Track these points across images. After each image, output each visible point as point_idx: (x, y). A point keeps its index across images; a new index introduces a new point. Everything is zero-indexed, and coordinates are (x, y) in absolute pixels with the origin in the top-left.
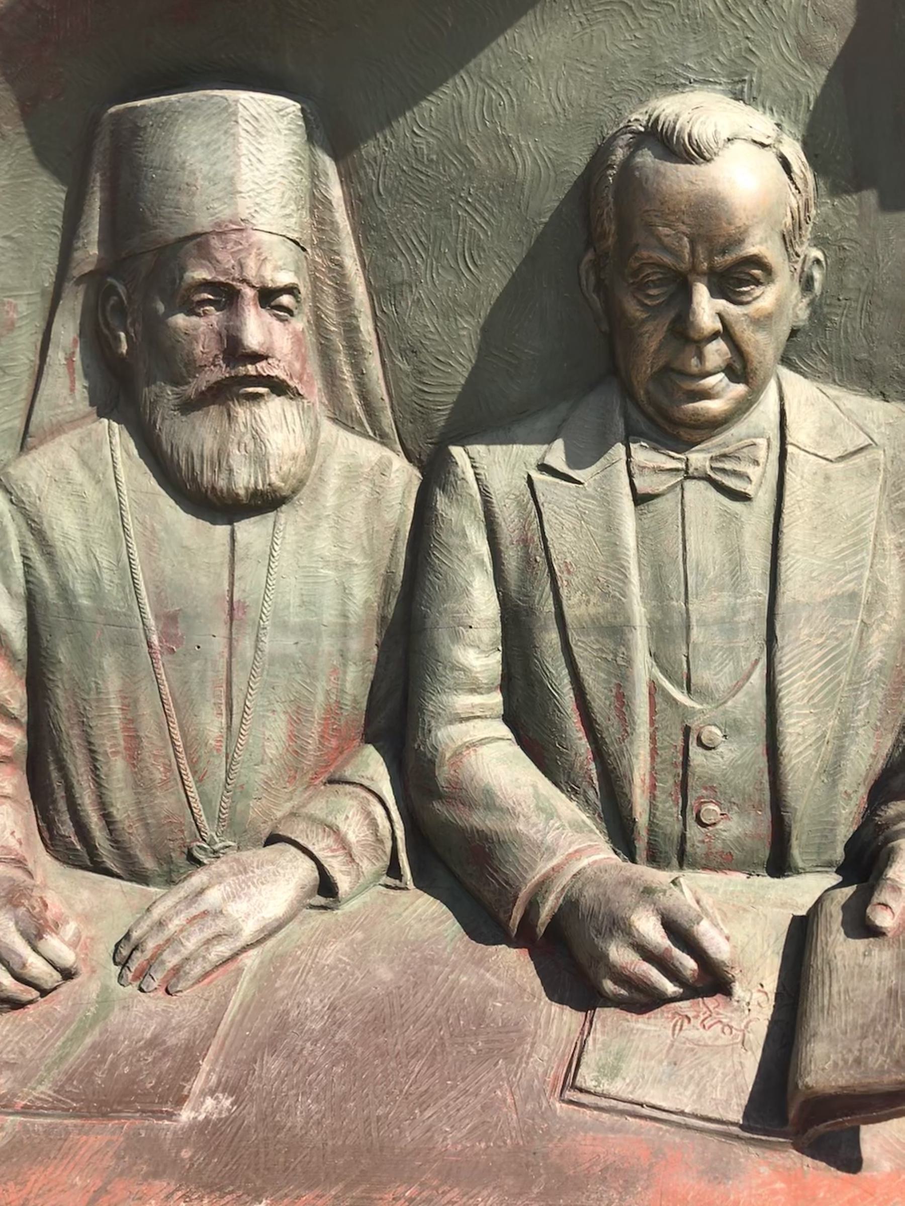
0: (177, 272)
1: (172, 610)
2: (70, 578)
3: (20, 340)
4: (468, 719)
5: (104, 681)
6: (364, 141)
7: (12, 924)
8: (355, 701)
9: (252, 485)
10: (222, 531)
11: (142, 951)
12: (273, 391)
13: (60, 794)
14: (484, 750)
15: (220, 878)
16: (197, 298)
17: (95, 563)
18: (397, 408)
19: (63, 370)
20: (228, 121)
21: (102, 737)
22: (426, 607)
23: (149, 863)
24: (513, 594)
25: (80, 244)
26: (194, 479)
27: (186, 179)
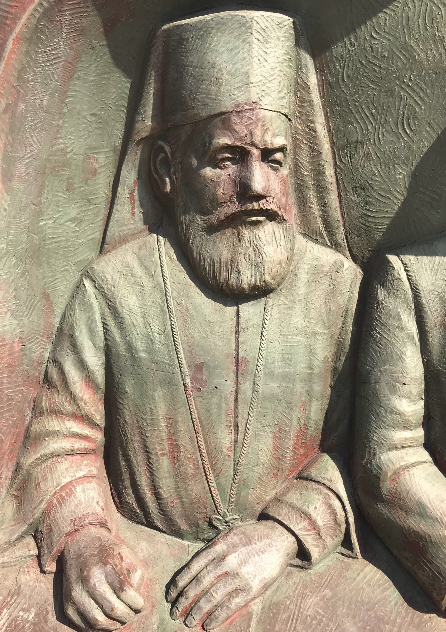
0: (207, 139)
1: (200, 362)
2: (134, 339)
3: (101, 181)
4: (402, 448)
5: (156, 407)
6: (335, 43)
7: (103, 577)
8: (316, 424)
9: (253, 282)
10: (231, 310)
11: (186, 598)
12: (267, 219)
13: (126, 476)
14: (414, 471)
15: (234, 547)
16: (220, 157)
17: (150, 330)
18: (347, 227)
19: (127, 201)
20: (246, 33)
21: (154, 443)
22: (370, 366)
23: (184, 526)
24: (435, 362)
25: (140, 118)
26: (214, 277)
27: (215, 75)
